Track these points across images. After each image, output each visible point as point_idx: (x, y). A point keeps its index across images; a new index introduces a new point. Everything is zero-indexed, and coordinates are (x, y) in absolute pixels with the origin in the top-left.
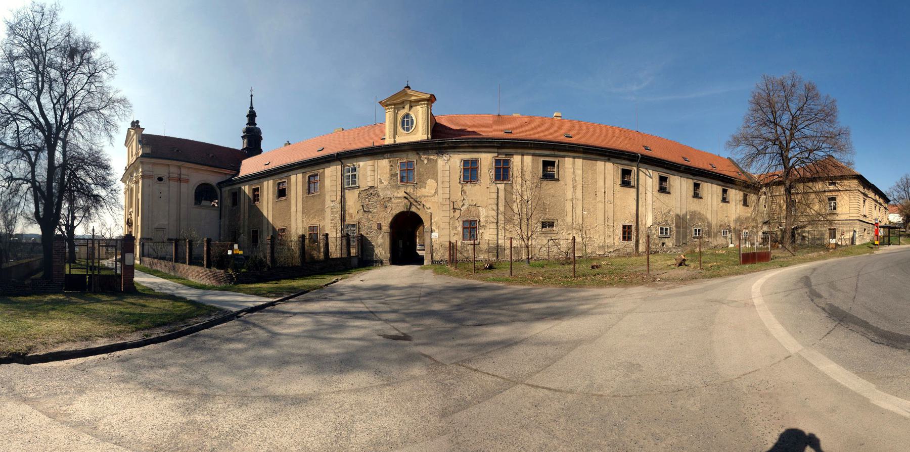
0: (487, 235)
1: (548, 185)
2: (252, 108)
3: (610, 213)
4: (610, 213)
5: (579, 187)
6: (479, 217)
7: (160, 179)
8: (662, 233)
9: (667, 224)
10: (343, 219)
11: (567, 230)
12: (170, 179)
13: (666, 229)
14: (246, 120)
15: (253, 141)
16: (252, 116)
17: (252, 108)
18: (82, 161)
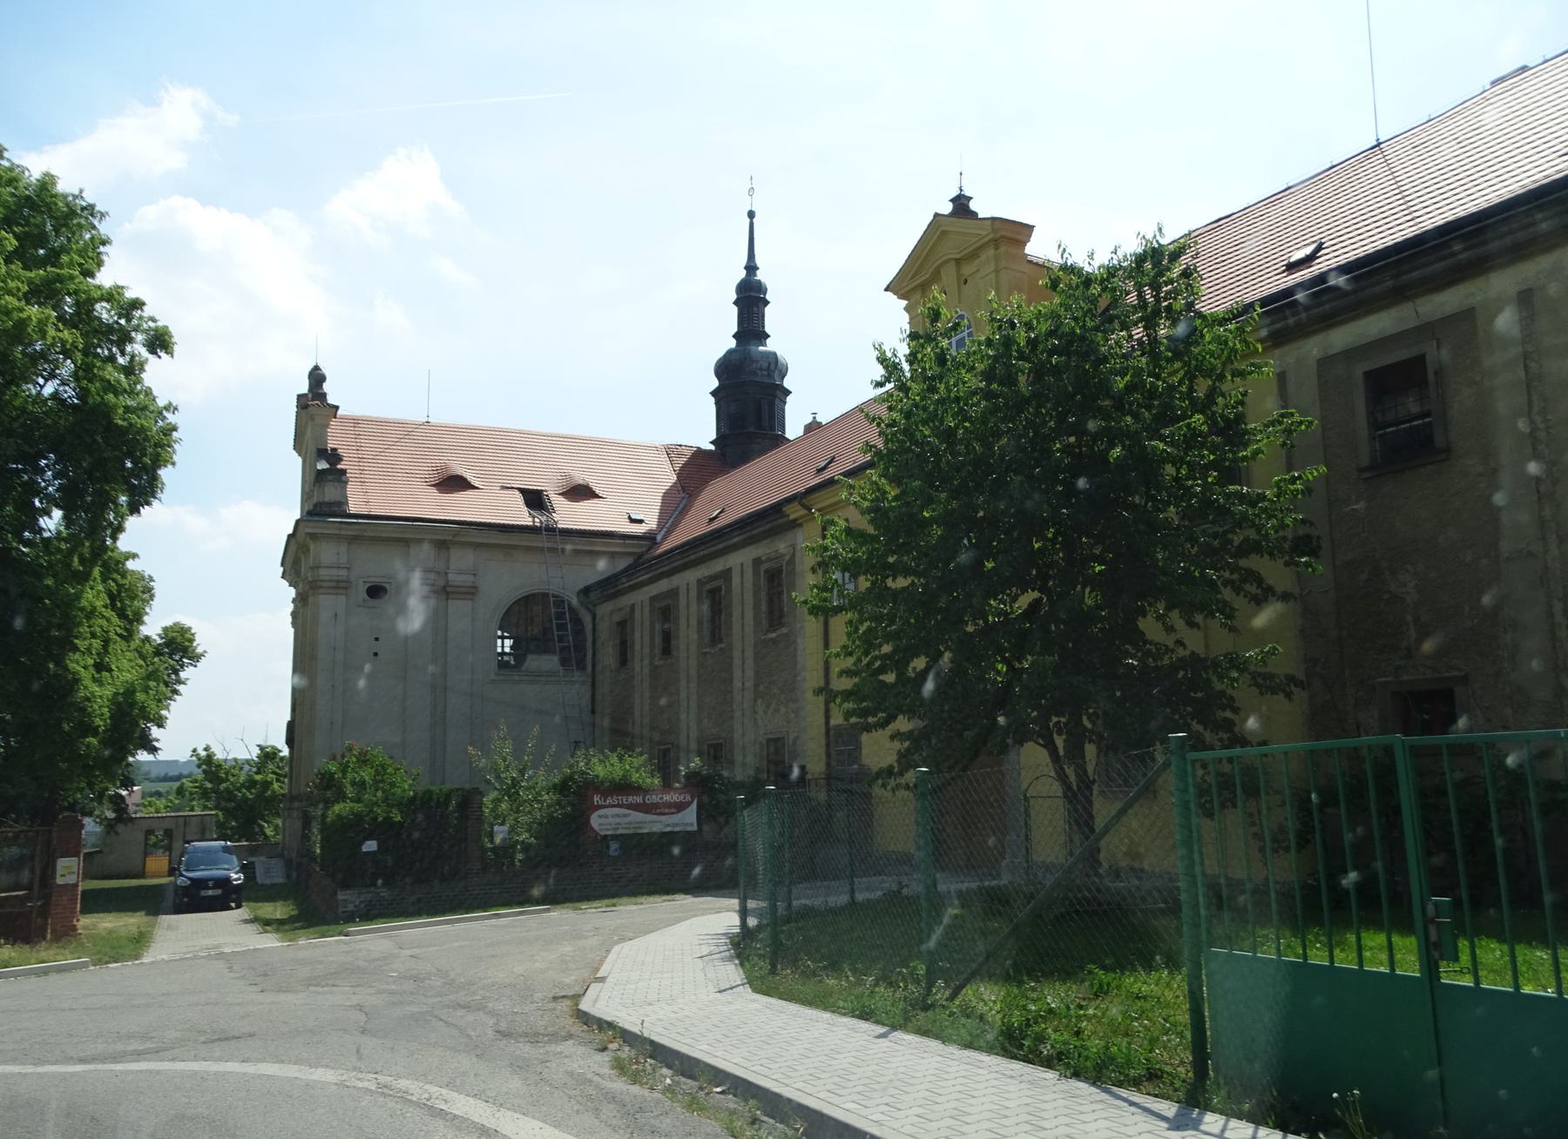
2: (751, 268)
15: (749, 390)
16: (751, 298)
17: (751, 268)
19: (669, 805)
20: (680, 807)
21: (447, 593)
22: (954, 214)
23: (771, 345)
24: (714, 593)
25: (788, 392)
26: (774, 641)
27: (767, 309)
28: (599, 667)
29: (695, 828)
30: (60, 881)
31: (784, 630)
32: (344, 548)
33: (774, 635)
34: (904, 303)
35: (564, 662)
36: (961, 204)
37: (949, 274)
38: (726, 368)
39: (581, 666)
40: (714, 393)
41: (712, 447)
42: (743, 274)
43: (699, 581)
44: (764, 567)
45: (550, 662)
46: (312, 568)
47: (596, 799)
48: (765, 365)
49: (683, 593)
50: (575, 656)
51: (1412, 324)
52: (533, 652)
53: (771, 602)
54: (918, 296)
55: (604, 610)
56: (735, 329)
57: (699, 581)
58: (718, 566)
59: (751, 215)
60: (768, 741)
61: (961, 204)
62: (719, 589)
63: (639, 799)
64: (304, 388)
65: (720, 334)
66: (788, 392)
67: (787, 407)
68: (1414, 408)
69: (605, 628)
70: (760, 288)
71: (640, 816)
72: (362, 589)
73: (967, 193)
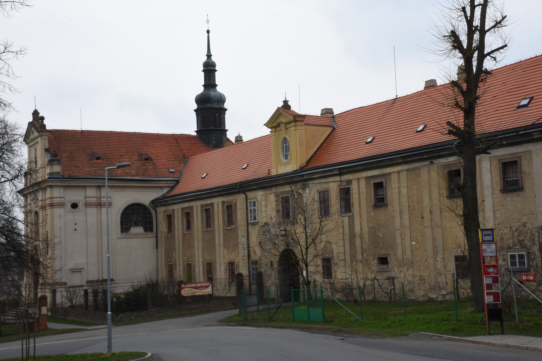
0: (341, 274)
1: (381, 214)
2: (209, 56)
3: (439, 242)
4: (439, 242)
5: (406, 211)
6: (332, 252)
7: (74, 206)
8: (513, 264)
9: (523, 247)
10: (249, 256)
11: (399, 266)
12: (87, 205)
13: (521, 257)
14: (201, 77)
15: (210, 109)
16: (209, 69)
17: (209, 56)
18: (14, 218)
19: (203, 287)
20: (207, 287)
21: (101, 205)
23: (218, 89)
24: (207, 211)
25: (226, 110)
27: (216, 73)
29: (211, 293)
31: (234, 227)
32: (62, 190)
35: (145, 230)
36: (286, 105)
37: (282, 127)
38: (200, 100)
39: (151, 230)
41: (195, 134)
42: (205, 59)
43: (201, 205)
44: (226, 205)
47: (183, 286)
49: (195, 208)
50: (148, 227)
51: (381, 173)
52: (133, 226)
53: (228, 215)
54: (274, 130)
55: (161, 210)
56: (203, 84)
57: (201, 205)
58: (209, 201)
59: (208, 32)
60: (229, 263)
61: (286, 105)
62: (209, 209)
63: (194, 285)
65: (198, 87)
66: (226, 110)
67: (226, 116)
68: (382, 193)
70: (213, 65)
71: (194, 290)
72: (69, 205)
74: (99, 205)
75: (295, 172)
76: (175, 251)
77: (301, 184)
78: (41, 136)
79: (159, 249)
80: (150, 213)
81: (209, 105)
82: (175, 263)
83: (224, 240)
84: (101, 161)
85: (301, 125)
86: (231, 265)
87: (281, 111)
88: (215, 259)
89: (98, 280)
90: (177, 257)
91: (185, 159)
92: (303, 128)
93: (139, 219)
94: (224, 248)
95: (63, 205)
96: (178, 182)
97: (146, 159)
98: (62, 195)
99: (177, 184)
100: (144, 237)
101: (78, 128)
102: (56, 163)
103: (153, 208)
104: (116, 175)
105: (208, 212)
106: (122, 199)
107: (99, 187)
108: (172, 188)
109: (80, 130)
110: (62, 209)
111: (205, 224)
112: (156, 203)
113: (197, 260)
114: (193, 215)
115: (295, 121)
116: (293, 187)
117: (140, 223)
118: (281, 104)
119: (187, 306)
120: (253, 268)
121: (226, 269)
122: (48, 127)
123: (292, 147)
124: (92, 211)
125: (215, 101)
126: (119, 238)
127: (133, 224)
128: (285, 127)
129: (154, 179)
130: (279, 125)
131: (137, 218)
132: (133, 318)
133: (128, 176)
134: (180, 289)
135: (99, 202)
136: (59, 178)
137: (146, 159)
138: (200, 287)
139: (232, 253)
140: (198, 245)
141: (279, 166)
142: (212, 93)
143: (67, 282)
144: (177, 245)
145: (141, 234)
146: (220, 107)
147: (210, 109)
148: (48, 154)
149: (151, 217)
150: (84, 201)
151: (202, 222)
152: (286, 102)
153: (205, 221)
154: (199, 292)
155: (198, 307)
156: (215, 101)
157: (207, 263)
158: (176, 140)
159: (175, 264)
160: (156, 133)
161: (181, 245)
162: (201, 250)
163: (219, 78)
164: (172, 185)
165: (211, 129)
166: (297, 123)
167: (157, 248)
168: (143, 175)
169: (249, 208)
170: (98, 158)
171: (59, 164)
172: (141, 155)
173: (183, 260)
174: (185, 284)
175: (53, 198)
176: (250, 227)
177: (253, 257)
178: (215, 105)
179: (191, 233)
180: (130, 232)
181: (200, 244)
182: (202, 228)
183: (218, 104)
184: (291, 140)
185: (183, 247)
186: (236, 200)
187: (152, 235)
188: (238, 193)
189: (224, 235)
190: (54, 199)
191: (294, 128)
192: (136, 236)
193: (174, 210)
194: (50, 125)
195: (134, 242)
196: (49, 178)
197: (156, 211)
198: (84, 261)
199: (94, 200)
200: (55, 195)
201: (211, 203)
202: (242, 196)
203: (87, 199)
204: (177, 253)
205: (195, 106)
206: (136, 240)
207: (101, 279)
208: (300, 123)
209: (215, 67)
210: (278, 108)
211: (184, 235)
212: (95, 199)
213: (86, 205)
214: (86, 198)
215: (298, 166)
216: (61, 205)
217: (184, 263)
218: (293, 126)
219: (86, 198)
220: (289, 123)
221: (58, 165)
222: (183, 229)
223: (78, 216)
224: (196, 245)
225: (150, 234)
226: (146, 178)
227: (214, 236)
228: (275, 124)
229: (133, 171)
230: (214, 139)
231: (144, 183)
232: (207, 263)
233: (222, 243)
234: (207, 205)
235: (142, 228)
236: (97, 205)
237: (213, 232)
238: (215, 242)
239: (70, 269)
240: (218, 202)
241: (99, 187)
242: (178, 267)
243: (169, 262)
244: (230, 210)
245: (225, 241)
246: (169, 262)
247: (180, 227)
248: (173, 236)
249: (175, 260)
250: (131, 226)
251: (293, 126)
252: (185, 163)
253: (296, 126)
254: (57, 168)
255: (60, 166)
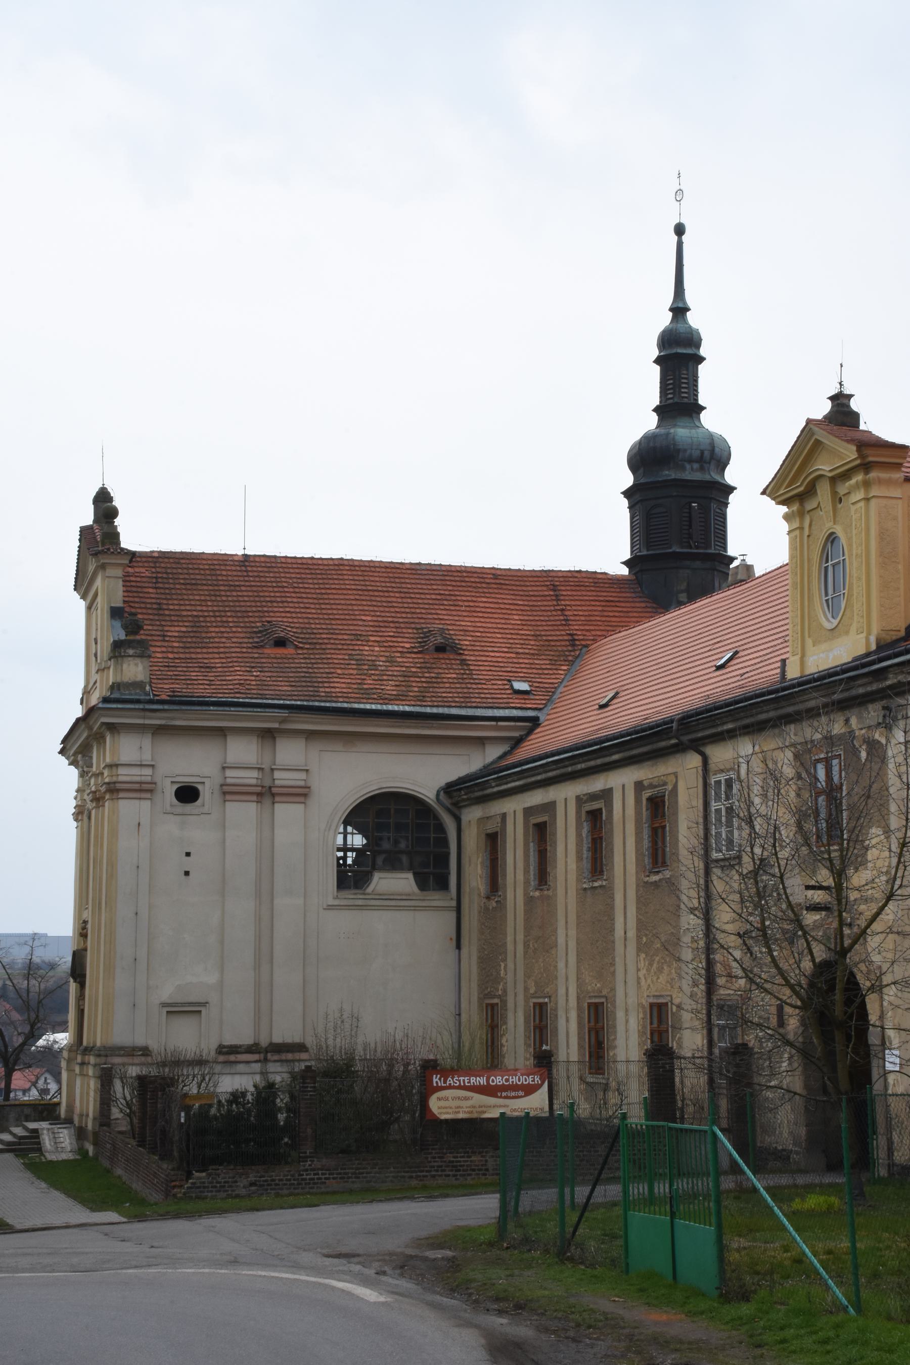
2: (679, 310)
7: (187, 794)
12: (228, 792)
16: (679, 356)
17: (679, 310)
19: (515, 1088)
20: (529, 1090)
21: (273, 795)
22: (830, 419)
23: (709, 421)
24: (595, 816)
25: (731, 489)
26: (656, 884)
28: (466, 889)
29: (547, 1114)
30: (498, 1195)
31: (667, 874)
32: (147, 741)
33: (655, 878)
34: (784, 509)
35: (423, 883)
36: (842, 412)
37: (824, 492)
38: (647, 458)
39: (443, 885)
40: (627, 494)
41: (625, 571)
42: (665, 319)
43: (578, 798)
44: (646, 794)
45: (400, 882)
46: (110, 766)
47: (436, 1080)
48: (698, 453)
50: (434, 872)
52: (382, 869)
54: (795, 507)
55: (472, 815)
56: (656, 402)
57: (578, 798)
58: (598, 784)
59: (680, 230)
60: (652, 1005)
61: (842, 412)
64: (87, 517)
66: (731, 489)
69: (472, 840)
70: (692, 340)
72: (170, 791)
73: (847, 392)
74: (267, 794)
75: (859, 663)
76: (505, 960)
77: (878, 706)
78: (103, 567)
79: (465, 951)
80: (440, 828)
81: (670, 474)
82: (503, 998)
83: (639, 921)
84: (289, 651)
85: (889, 482)
86: (659, 1014)
87: (820, 434)
88: (613, 989)
89: (256, 1045)
90: (510, 978)
91: (574, 650)
92: (897, 493)
93: (403, 845)
94: (639, 950)
95: (151, 791)
96: (535, 722)
97: (440, 649)
98: (147, 757)
99: (530, 731)
100: (415, 908)
101: (234, 548)
102: (131, 652)
103: (449, 810)
104: (329, 697)
105: (595, 819)
106: (349, 774)
107: (268, 735)
108: (517, 742)
109: (240, 552)
110: (146, 804)
111: (587, 865)
112: (460, 793)
113: (562, 991)
114: (554, 834)
115: (866, 467)
116: (854, 721)
117: (405, 859)
118: (822, 409)
119: (450, 1157)
120: (722, 1028)
121: (644, 1027)
122: (129, 541)
123: (854, 568)
124: (244, 813)
125: (690, 461)
126: (330, 907)
127: (380, 860)
128: (834, 493)
129: (454, 711)
130: (810, 491)
131: (396, 842)
132: (243, 1192)
133: (369, 700)
134: (427, 1091)
135: (267, 783)
136: (138, 701)
137: (440, 649)
138: (503, 1088)
139: (660, 970)
140: (566, 937)
141: (809, 642)
142: (681, 432)
143: (153, 1045)
144: (509, 939)
145: (407, 897)
146: (707, 477)
147: (675, 488)
148: (118, 624)
149: (445, 842)
150: (218, 780)
151: (579, 858)
152: (840, 401)
153: (586, 854)
154: (493, 1108)
155: (491, 1163)
156: (690, 461)
157: (589, 1005)
158: (554, 588)
159: (504, 1003)
160: (488, 564)
161: (520, 937)
162: (572, 959)
163: (709, 384)
164: (516, 734)
165: (674, 552)
166: (873, 475)
167: (459, 946)
168: (420, 699)
169: (714, 806)
170: (280, 643)
171: (141, 656)
172: (428, 634)
173: (526, 989)
174: (446, 1073)
175: (117, 766)
176: (717, 871)
177: (726, 991)
178: (691, 474)
179: (548, 897)
180: (370, 889)
181: (573, 932)
182: (579, 881)
183: (702, 469)
184: (850, 539)
185: (526, 945)
186: (676, 775)
187: (446, 900)
188: (679, 749)
189: (641, 902)
190: (121, 771)
191: (859, 495)
192: (391, 902)
193: (504, 816)
194: (136, 534)
195: (381, 924)
196: (105, 700)
197: (458, 820)
198: (212, 978)
199: (251, 777)
200: (124, 759)
201: (603, 791)
202: (693, 761)
203: (229, 773)
204: (511, 965)
205: (628, 479)
206: (387, 915)
207: (264, 1043)
208: (884, 475)
209: (698, 344)
210: (809, 422)
211: (529, 901)
212: (255, 774)
213: (224, 793)
214: (224, 768)
215: (873, 639)
216: (144, 790)
217: (526, 1001)
218: (857, 486)
219: (224, 768)
220: (845, 475)
221: (138, 660)
222: (527, 882)
223: (196, 828)
224: (561, 940)
225: (436, 898)
226: (428, 710)
227: (612, 907)
228: (799, 487)
229: (390, 688)
230: (683, 586)
231: (419, 727)
232: (589, 1005)
233: (632, 933)
234: (593, 797)
235: (410, 876)
236: (259, 794)
237: (608, 890)
238: (612, 930)
239: (164, 1005)
240: (622, 782)
241: (268, 735)
242: (510, 1015)
243: (490, 995)
244: (657, 807)
245: (641, 926)
246: (490, 995)
247: (520, 877)
248: (501, 905)
249: (505, 991)
250: (374, 868)
251: (857, 486)
252: (572, 663)
253: (867, 484)
254: (135, 670)
255: (146, 662)
